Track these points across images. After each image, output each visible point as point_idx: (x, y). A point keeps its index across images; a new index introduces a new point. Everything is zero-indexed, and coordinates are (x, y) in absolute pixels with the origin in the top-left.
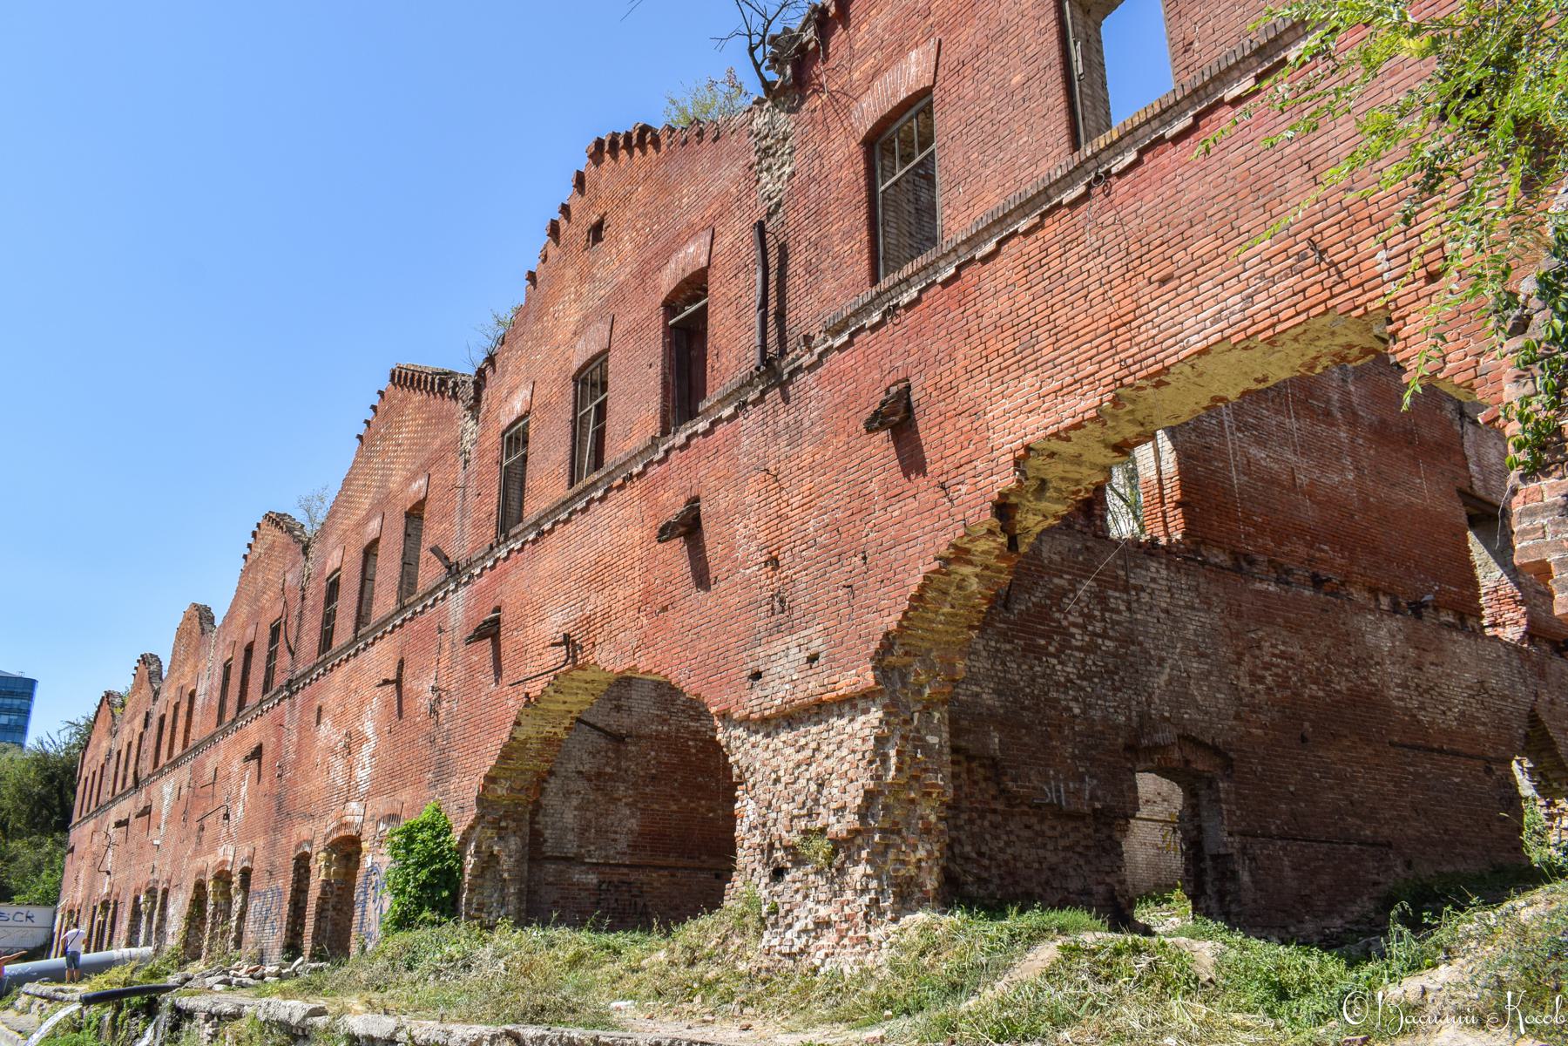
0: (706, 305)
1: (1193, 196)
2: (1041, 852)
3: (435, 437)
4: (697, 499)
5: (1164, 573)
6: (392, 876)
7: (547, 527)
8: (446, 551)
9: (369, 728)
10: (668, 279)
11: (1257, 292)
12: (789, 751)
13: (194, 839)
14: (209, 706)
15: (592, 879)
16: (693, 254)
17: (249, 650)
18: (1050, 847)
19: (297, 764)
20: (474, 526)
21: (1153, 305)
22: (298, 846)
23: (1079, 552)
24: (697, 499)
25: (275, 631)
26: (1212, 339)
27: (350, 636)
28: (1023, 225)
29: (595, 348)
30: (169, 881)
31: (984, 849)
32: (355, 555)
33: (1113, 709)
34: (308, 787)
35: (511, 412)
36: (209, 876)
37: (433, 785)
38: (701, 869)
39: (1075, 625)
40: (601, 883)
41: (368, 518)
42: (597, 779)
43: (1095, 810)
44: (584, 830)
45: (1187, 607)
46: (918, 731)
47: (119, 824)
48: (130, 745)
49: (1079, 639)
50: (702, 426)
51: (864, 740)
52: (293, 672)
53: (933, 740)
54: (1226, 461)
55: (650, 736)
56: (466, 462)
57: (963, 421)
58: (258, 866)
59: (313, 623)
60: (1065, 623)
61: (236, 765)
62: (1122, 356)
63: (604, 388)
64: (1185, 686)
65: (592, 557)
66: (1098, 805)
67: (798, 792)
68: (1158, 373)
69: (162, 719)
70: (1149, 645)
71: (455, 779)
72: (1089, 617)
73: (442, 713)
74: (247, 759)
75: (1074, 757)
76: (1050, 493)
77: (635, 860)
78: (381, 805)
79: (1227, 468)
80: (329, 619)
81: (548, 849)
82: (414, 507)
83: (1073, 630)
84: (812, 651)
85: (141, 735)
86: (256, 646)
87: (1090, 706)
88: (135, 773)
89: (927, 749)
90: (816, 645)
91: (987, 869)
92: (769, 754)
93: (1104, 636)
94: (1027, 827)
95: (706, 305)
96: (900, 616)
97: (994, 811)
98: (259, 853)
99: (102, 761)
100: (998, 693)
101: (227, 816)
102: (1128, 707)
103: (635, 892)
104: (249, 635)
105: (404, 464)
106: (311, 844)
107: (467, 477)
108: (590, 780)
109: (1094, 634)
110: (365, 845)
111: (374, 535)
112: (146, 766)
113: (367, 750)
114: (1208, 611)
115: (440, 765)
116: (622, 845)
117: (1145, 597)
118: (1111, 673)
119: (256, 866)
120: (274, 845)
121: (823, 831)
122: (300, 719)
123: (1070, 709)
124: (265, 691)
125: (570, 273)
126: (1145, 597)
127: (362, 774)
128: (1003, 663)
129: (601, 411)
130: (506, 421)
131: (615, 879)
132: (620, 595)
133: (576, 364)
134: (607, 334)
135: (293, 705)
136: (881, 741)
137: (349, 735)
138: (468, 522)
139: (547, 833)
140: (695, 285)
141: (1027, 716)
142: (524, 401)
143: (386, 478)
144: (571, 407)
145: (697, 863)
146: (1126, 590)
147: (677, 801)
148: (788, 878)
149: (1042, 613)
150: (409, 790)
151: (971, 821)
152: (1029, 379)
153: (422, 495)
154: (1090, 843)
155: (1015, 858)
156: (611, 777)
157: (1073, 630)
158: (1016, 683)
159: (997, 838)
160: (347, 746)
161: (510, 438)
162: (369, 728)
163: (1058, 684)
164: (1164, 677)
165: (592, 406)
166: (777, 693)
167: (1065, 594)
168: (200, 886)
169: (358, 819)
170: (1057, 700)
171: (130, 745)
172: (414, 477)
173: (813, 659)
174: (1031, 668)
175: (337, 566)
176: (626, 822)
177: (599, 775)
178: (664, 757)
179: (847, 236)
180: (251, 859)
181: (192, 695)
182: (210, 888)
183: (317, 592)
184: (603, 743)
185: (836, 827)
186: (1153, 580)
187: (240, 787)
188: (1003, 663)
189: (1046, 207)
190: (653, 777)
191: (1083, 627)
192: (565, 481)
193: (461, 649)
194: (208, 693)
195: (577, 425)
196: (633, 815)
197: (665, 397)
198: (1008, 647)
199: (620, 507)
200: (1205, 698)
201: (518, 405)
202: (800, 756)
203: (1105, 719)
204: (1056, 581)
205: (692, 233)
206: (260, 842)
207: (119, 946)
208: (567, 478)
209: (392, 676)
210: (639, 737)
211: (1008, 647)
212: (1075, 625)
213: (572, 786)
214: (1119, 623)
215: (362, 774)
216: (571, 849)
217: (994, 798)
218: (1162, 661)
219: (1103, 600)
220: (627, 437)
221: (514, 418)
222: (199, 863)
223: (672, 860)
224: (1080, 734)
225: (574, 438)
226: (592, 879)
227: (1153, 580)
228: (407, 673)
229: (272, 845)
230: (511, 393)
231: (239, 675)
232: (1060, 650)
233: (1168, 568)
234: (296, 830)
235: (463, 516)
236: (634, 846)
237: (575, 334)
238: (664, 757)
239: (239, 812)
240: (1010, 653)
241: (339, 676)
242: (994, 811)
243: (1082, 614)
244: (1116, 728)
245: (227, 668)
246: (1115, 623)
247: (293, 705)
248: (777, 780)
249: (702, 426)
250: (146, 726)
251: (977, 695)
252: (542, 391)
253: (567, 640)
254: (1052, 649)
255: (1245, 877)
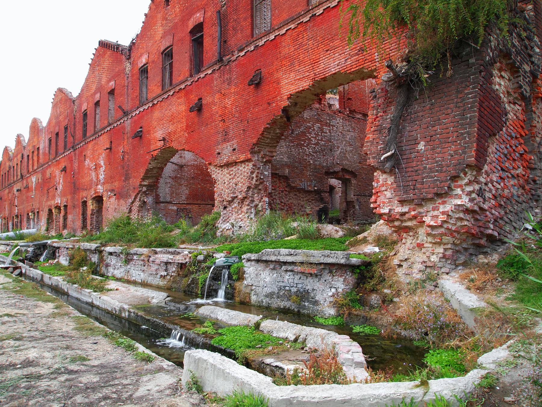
0: (203, 35)
1: (336, 26)
2: (299, 201)
3: (116, 67)
4: (201, 99)
5: (341, 121)
6: (502, 359)
7: (155, 102)
8: (123, 107)
9: (102, 163)
10: (191, 24)
11: (348, 59)
12: (228, 175)
13: (46, 195)
14: (45, 152)
15: (175, 208)
16: (198, 17)
17: (57, 134)
18: (302, 200)
19: (79, 173)
20: (132, 100)
21: (324, 58)
22: (82, 198)
23: (315, 115)
24: (201, 99)
25: (66, 129)
26: (337, 71)
27: (93, 132)
28: (292, 26)
29: (168, 44)
30: (39, 209)
31: (283, 201)
32: (92, 105)
33: (325, 161)
34: (84, 181)
35: (142, 62)
36: (53, 207)
37: (124, 181)
38: (209, 205)
39: (313, 137)
40: (178, 209)
41: (95, 93)
42: (175, 178)
43: (315, 190)
44: (172, 194)
45: (348, 131)
46: (262, 171)
47: (18, 190)
48: (17, 164)
49: (314, 141)
50: (202, 76)
51: (247, 173)
52: (74, 143)
53: (266, 173)
54: (365, 86)
55: (191, 165)
56: (128, 77)
57: (275, 85)
58: (70, 204)
59: (79, 127)
60: (310, 137)
61: (57, 173)
62: (315, 72)
63: (172, 59)
64: (345, 154)
65: (170, 114)
66: (316, 188)
67: (230, 187)
68: (324, 78)
69: (28, 156)
70: (335, 142)
71: (131, 180)
72: (317, 135)
73: (126, 159)
74: (62, 171)
75: (310, 175)
76: (298, 106)
77: (188, 202)
78: (108, 186)
79: (365, 88)
80: (85, 126)
81: (161, 199)
82: (111, 91)
83: (312, 139)
84: (234, 147)
85: (21, 161)
86: (59, 134)
87: (316, 161)
88: (21, 174)
89: (264, 175)
90: (235, 146)
91: (283, 206)
92: (222, 176)
93: (322, 140)
94: (295, 195)
95: (203, 35)
96: (257, 139)
97: (286, 191)
98: (69, 201)
99: (8, 169)
100: (289, 158)
101: (56, 189)
102: (327, 161)
103: (188, 211)
104: (57, 130)
105: (106, 75)
106: (86, 198)
107: (128, 83)
108: (173, 179)
109: (318, 140)
110: (104, 199)
111: (98, 100)
112: (24, 172)
113: (102, 169)
114: (354, 132)
115: (126, 175)
116: (184, 197)
117: (335, 129)
118: (322, 151)
119: (69, 205)
120: (74, 198)
121: (237, 197)
122: (79, 158)
123: (310, 162)
124: (65, 149)
125: (159, 16)
126: (335, 129)
127: (101, 177)
128: (290, 149)
129: (171, 65)
130: (140, 65)
131: (182, 208)
132: (179, 127)
133: (162, 49)
134: (172, 40)
135: (75, 154)
136: (252, 173)
137: (96, 165)
138: (130, 98)
139: (161, 195)
140: (199, 28)
141: (297, 164)
142: (146, 59)
143: (100, 80)
144: (161, 63)
145: (207, 203)
146: (329, 127)
147: (200, 185)
148: (228, 209)
149: (303, 134)
150: (117, 182)
151: (279, 193)
152: (292, 75)
153: (113, 87)
154: (313, 198)
155: (291, 203)
156: (180, 178)
157: (312, 139)
158: (294, 155)
159: (286, 198)
160: (96, 168)
161: (142, 71)
162: (102, 163)
163: (307, 154)
164: (339, 152)
165: (168, 63)
166: (225, 159)
167: (310, 128)
168: (50, 211)
169: (101, 191)
170: (306, 159)
171: (17, 164)
172: (110, 81)
173: (234, 150)
174: (299, 150)
175: (86, 108)
176: (185, 191)
177: (176, 177)
178: (196, 171)
179: (245, 19)
180: (67, 202)
181: (38, 148)
182: (53, 211)
183: (79, 117)
184: (177, 167)
185: (240, 196)
186: (338, 123)
187: (60, 180)
188: (290, 149)
189: (299, 22)
190: (193, 178)
191: (315, 138)
192: (160, 88)
193: (131, 140)
194: (44, 148)
195: (164, 69)
196: (187, 189)
197: (191, 64)
198: (292, 144)
199: (178, 98)
200: (350, 157)
201: (144, 60)
202: (230, 177)
203: (320, 165)
204: (308, 124)
205: (198, 10)
206: (69, 197)
207: (24, 229)
208: (161, 87)
209: (108, 146)
210: (188, 166)
211: (292, 144)
212: (313, 137)
213: (168, 181)
214: (326, 136)
215: (101, 177)
216: (168, 200)
217: (286, 187)
218: (338, 147)
219: (321, 130)
220: (179, 76)
221: (143, 64)
222: (49, 203)
223: (199, 202)
224: (312, 169)
225: (163, 73)
226: (175, 208)
227: (338, 123)
228: (113, 145)
229: (73, 198)
230: (141, 56)
231: (55, 143)
232: (308, 145)
233: (343, 119)
234: (81, 193)
235: (128, 96)
236: (187, 198)
237: (161, 38)
238: (196, 171)
239: (60, 188)
240: (293, 146)
241: (90, 146)
242: (286, 191)
243: (315, 134)
244: (323, 167)
245: (50, 140)
246: (325, 136)
247: (75, 154)
248: (225, 183)
249: (202, 76)
250: (22, 159)
251: (282, 159)
252: (152, 56)
253: (164, 139)
254: (305, 145)
255: (357, 207)
